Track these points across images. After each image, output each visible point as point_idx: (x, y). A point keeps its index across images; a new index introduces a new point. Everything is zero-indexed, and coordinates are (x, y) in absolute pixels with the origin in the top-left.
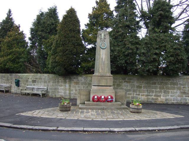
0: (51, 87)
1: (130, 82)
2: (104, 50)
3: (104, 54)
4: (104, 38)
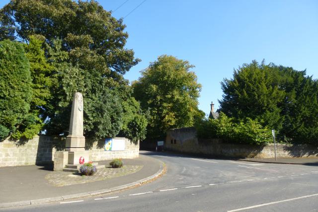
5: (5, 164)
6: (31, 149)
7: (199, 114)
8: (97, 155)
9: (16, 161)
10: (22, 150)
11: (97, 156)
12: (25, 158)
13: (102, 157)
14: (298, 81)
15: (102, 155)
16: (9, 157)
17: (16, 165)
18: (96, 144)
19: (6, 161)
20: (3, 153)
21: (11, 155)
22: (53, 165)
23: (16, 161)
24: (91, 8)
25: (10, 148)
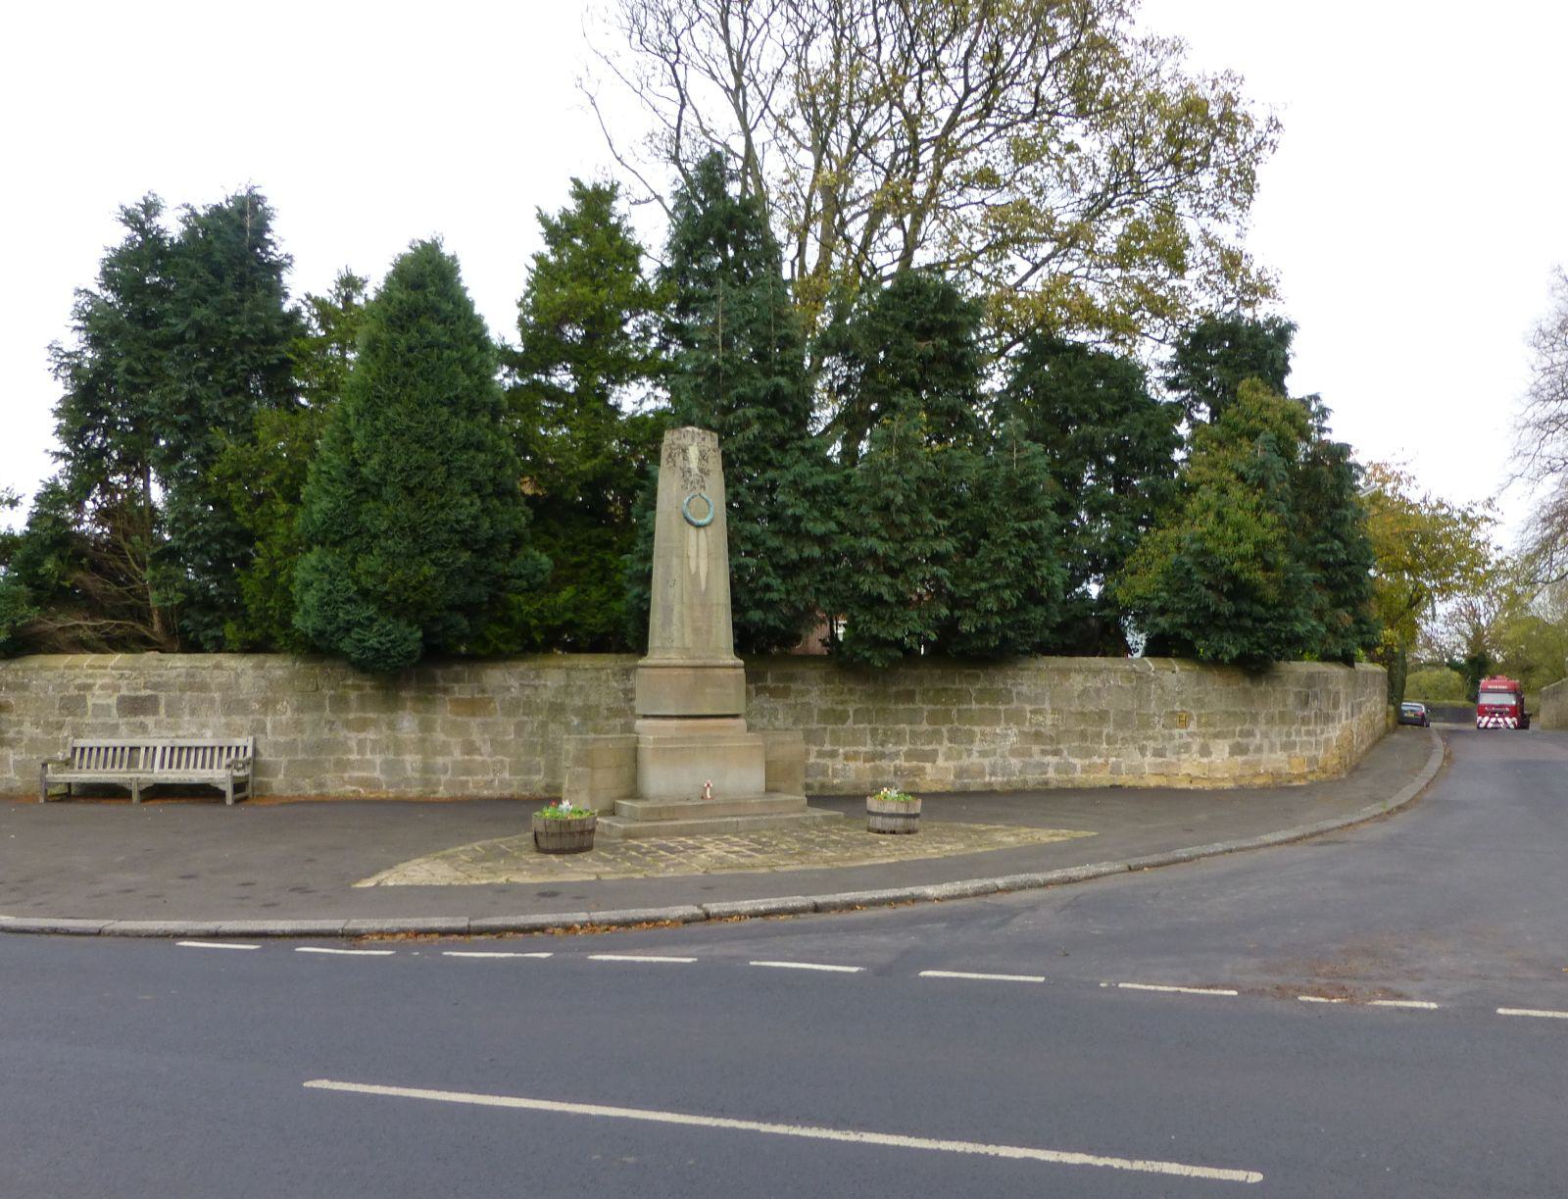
0: (282, 739)
1: (785, 693)
2: (702, 531)
3: (703, 555)
4: (701, 470)
5: (464, 784)
6: (567, 725)
7: (1331, 480)
8: (931, 757)
9: (506, 775)
10: (529, 728)
11: (928, 766)
12: (541, 761)
13: (961, 773)
14: (143, 713)
15: (965, 761)
16: (477, 758)
17: (507, 793)
18: (651, 232)
19: (468, 772)
20: (453, 740)
21: (487, 748)
22: (736, 646)
23: (506, 775)
24: (138, 219)
25: (479, 720)
